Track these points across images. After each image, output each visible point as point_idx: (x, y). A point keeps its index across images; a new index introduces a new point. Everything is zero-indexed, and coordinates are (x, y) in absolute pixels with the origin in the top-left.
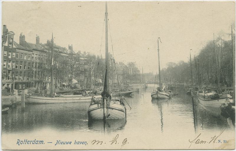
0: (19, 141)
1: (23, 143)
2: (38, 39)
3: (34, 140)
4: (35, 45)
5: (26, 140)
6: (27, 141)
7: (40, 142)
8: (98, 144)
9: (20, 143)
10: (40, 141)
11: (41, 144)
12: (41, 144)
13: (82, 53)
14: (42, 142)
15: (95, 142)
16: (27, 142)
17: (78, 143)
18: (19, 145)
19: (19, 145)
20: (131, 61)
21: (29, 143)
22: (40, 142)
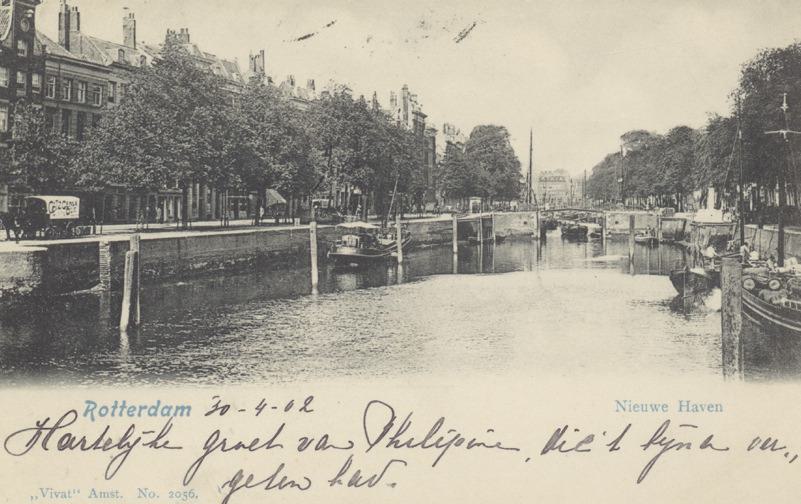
0: (92, 406)
1: (109, 414)
2: (131, 31)
3: (155, 404)
4: (117, 45)
5: (120, 404)
6: (128, 405)
7: (180, 411)
8: (642, 483)
9: (96, 412)
10: (178, 408)
11: (121, 414)
12: (121, 414)
13: (301, 83)
14: (186, 410)
15: (425, 441)
16: (125, 410)
17: (152, 411)
18: (93, 419)
19: (93, 419)
20: (486, 120)
21: (136, 413)
22: (180, 411)
